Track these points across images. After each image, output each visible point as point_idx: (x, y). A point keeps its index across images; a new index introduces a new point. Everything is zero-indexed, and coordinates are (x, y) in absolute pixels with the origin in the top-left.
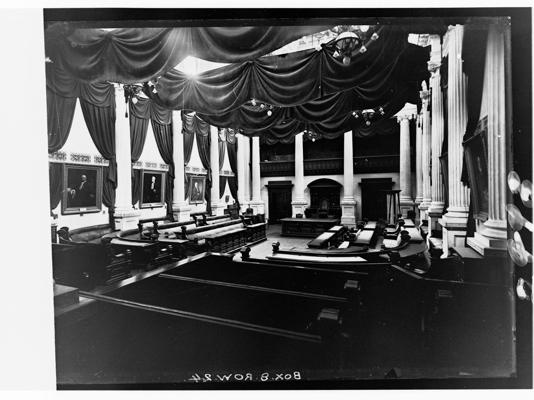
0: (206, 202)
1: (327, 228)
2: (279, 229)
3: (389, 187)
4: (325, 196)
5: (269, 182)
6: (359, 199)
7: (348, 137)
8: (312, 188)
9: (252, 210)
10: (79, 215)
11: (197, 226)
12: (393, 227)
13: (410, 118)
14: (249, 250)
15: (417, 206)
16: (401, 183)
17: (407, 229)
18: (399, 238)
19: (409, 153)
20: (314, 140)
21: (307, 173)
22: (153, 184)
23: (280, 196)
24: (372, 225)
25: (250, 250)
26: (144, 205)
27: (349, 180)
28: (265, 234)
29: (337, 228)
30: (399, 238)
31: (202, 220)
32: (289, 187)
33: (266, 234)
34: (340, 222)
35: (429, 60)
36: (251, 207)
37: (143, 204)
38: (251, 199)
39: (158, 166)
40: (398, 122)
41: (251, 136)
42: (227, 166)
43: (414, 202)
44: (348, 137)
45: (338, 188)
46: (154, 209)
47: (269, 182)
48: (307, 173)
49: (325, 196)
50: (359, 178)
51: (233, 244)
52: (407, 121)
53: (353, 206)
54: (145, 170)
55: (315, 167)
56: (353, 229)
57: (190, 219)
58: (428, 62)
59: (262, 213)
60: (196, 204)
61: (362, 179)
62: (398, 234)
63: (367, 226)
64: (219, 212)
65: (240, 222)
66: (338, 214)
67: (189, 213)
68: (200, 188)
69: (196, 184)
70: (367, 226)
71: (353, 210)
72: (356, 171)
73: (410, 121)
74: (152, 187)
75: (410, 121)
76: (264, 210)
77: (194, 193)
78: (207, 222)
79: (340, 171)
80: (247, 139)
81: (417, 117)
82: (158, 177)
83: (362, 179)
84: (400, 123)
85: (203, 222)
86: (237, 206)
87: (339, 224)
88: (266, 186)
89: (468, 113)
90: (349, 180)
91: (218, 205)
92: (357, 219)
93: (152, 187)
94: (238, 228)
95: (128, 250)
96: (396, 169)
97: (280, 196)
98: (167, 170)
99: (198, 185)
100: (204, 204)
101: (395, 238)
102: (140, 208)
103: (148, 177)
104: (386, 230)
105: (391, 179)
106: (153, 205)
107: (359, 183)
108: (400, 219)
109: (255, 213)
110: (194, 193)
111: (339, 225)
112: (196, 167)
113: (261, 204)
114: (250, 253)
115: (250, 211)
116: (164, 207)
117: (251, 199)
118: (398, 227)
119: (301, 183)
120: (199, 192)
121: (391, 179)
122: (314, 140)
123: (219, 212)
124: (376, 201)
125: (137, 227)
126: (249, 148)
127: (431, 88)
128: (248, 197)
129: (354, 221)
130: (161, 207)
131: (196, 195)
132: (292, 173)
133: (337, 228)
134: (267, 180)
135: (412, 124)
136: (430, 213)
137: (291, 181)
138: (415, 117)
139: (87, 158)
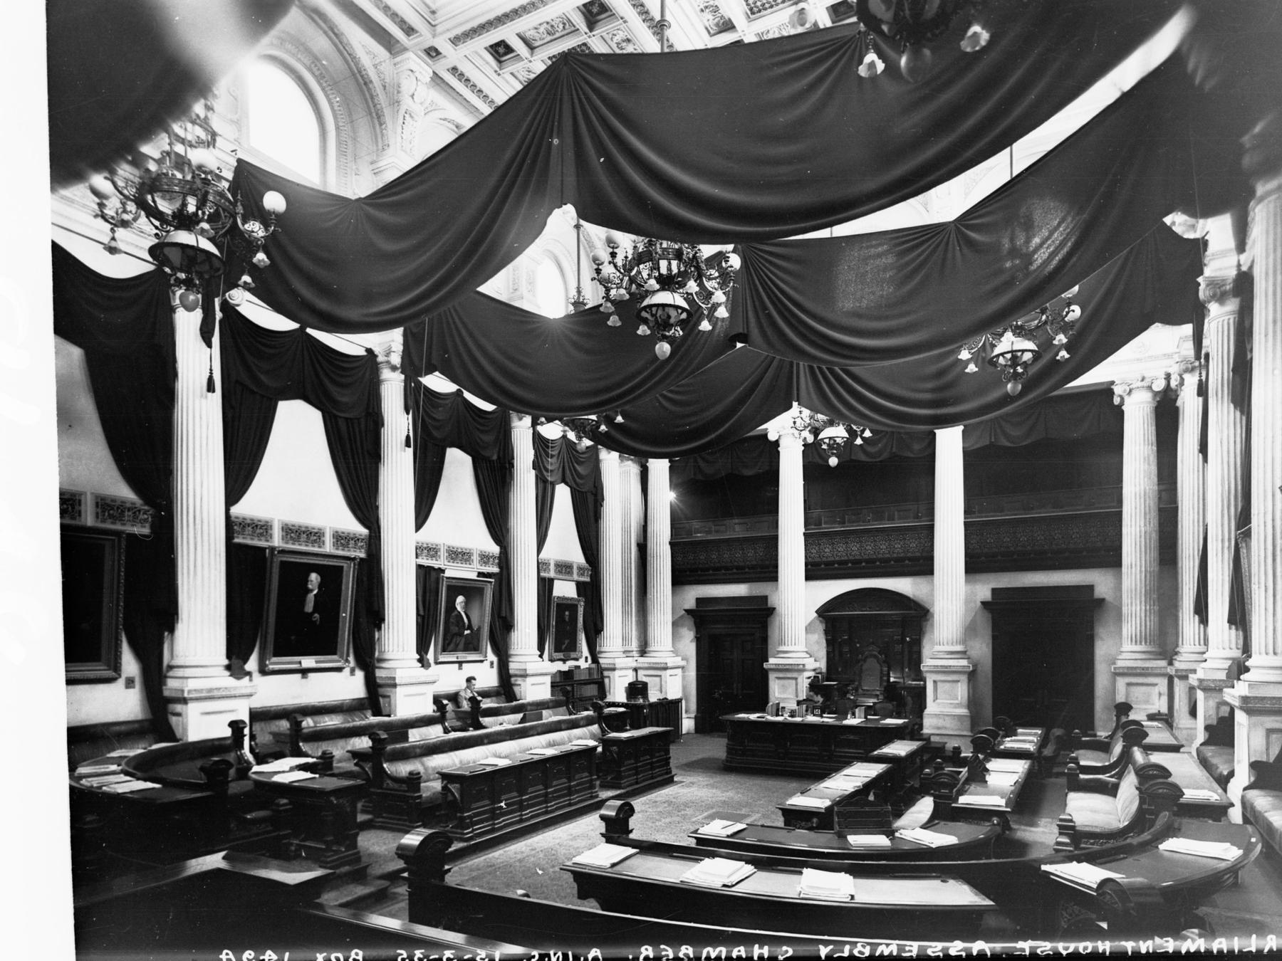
0: (491, 657)
1: (864, 744)
2: (716, 748)
3: (1080, 617)
4: (874, 638)
5: (699, 601)
6: (982, 649)
7: (950, 446)
8: (832, 617)
9: (645, 685)
10: (299, 676)
11: (446, 731)
12: (1105, 747)
13: (1159, 385)
14: (627, 811)
15: (1186, 678)
16: (1126, 599)
17: (1157, 758)
18: (1129, 785)
19: (1152, 503)
20: (833, 461)
21: (815, 571)
22: (311, 597)
23: (733, 645)
24: (1027, 739)
25: (631, 811)
26: (275, 663)
27: (951, 596)
28: (667, 761)
29: (900, 748)
30: (1129, 785)
31: (463, 716)
32: (759, 617)
33: (673, 763)
34: (921, 727)
35: (1202, 273)
36: (642, 678)
37: (275, 659)
38: (643, 652)
39: (328, 539)
40: (1116, 401)
41: (641, 457)
42: (564, 542)
43: (1171, 664)
44: (950, 446)
45: (915, 616)
46: (311, 675)
47: (699, 601)
48: (815, 571)
49: (874, 638)
50: (983, 591)
51: (546, 795)
52: (1148, 396)
53: (964, 678)
54: (283, 552)
55: (840, 551)
56: (957, 750)
57: (429, 709)
58: (1200, 279)
59: (673, 693)
60: (460, 663)
61: (993, 590)
62: (1120, 776)
63: (1009, 744)
64: (535, 689)
65: (589, 722)
66: (910, 701)
67: (430, 691)
68: (481, 617)
69: (460, 599)
70: (1009, 744)
71: (962, 690)
72: (975, 564)
73: (1156, 394)
74: (309, 607)
75: (1156, 394)
76: (684, 688)
77: (454, 629)
78: (485, 721)
79: (923, 565)
80: (633, 468)
81: (1182, 383)
82: (331, 574)
83: (994, 591)
84: (1122, 403)
85: (473, 717)
86: (598, 679)
87: (912, 731)
88: (688, 611)
89: (1177, 590)
90: (951, 596)
91: (531, 669)
92: (974, 718)
93: (309, 607)
94: (583, 738)
95: (285, 801)
96: (1111, 558)
97: (733, 645)
98: (363, 555)
99: (467, 605)
100: (487, 664)
101: (1111, 790)
102: (264, 671)
103: (295, 571)
104: (1075, 760)
105: (1090, 588)
106: (308, 662)
107: (985, 604)
108: (1124, 719)
109: (653, 697)
110: (454, 629)
111: (912, 739)
112: (460, 543)
113: (674, 672)
114: (633, 823)
115: (637, 689)
116: (487, 664)
117: (643, 652)
118: (1118, 749)
119: (799, 600)
120: (470, 627)
121: (1090, 588)
122: (833, 461)
123: (535, 689)
124: (1040, 663)
125: (228, 732)
126: (640, 495)
127: (1207, 356)
128: (634, 645)
129: (967, 723)
130: (339, 669)
131: (461, 634)
132: (769, 571)
133: (900, 748)
134: (693, 594)
135: (1166, 412)
136: (1245, 699)
137: (765, 598)
138: (1173, 384)
139: (314, 535)
